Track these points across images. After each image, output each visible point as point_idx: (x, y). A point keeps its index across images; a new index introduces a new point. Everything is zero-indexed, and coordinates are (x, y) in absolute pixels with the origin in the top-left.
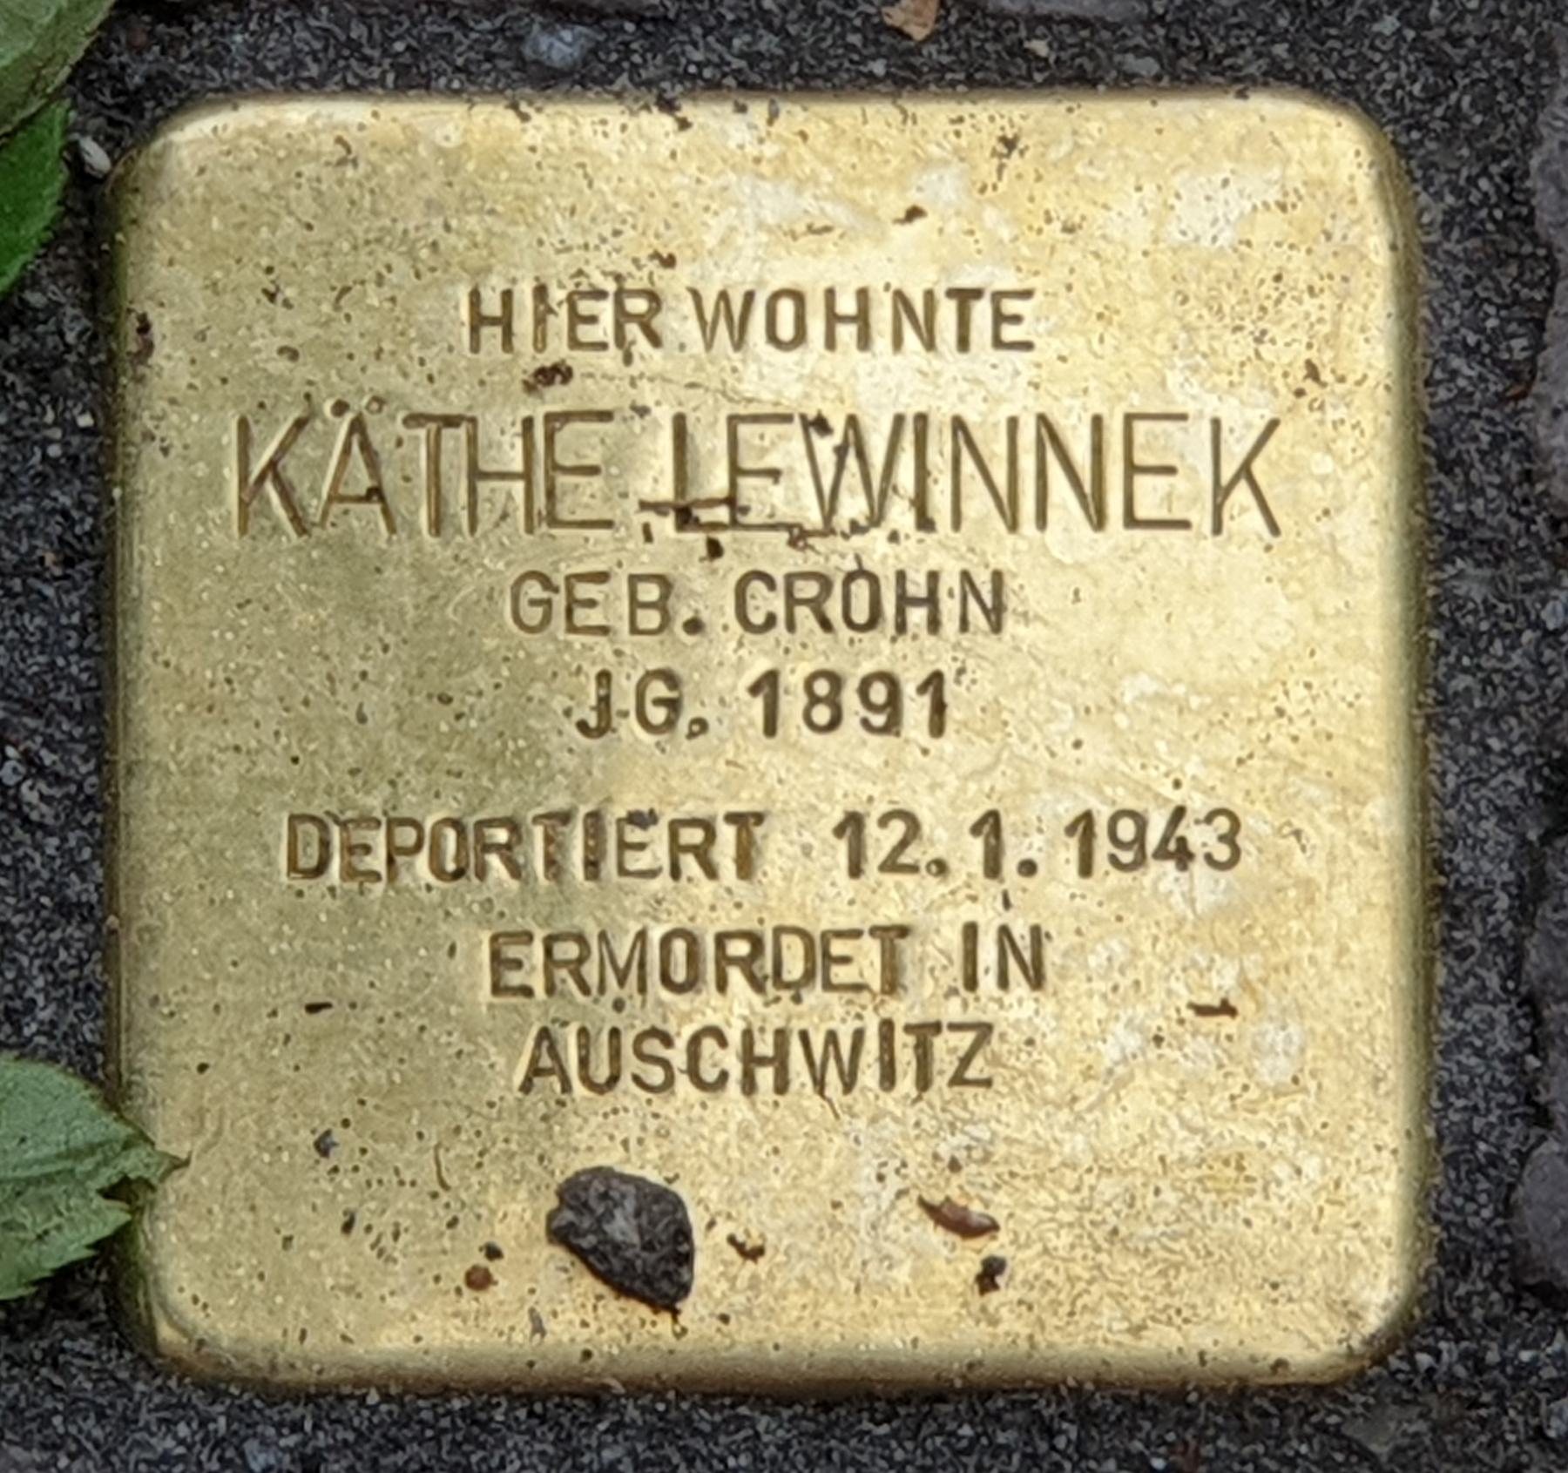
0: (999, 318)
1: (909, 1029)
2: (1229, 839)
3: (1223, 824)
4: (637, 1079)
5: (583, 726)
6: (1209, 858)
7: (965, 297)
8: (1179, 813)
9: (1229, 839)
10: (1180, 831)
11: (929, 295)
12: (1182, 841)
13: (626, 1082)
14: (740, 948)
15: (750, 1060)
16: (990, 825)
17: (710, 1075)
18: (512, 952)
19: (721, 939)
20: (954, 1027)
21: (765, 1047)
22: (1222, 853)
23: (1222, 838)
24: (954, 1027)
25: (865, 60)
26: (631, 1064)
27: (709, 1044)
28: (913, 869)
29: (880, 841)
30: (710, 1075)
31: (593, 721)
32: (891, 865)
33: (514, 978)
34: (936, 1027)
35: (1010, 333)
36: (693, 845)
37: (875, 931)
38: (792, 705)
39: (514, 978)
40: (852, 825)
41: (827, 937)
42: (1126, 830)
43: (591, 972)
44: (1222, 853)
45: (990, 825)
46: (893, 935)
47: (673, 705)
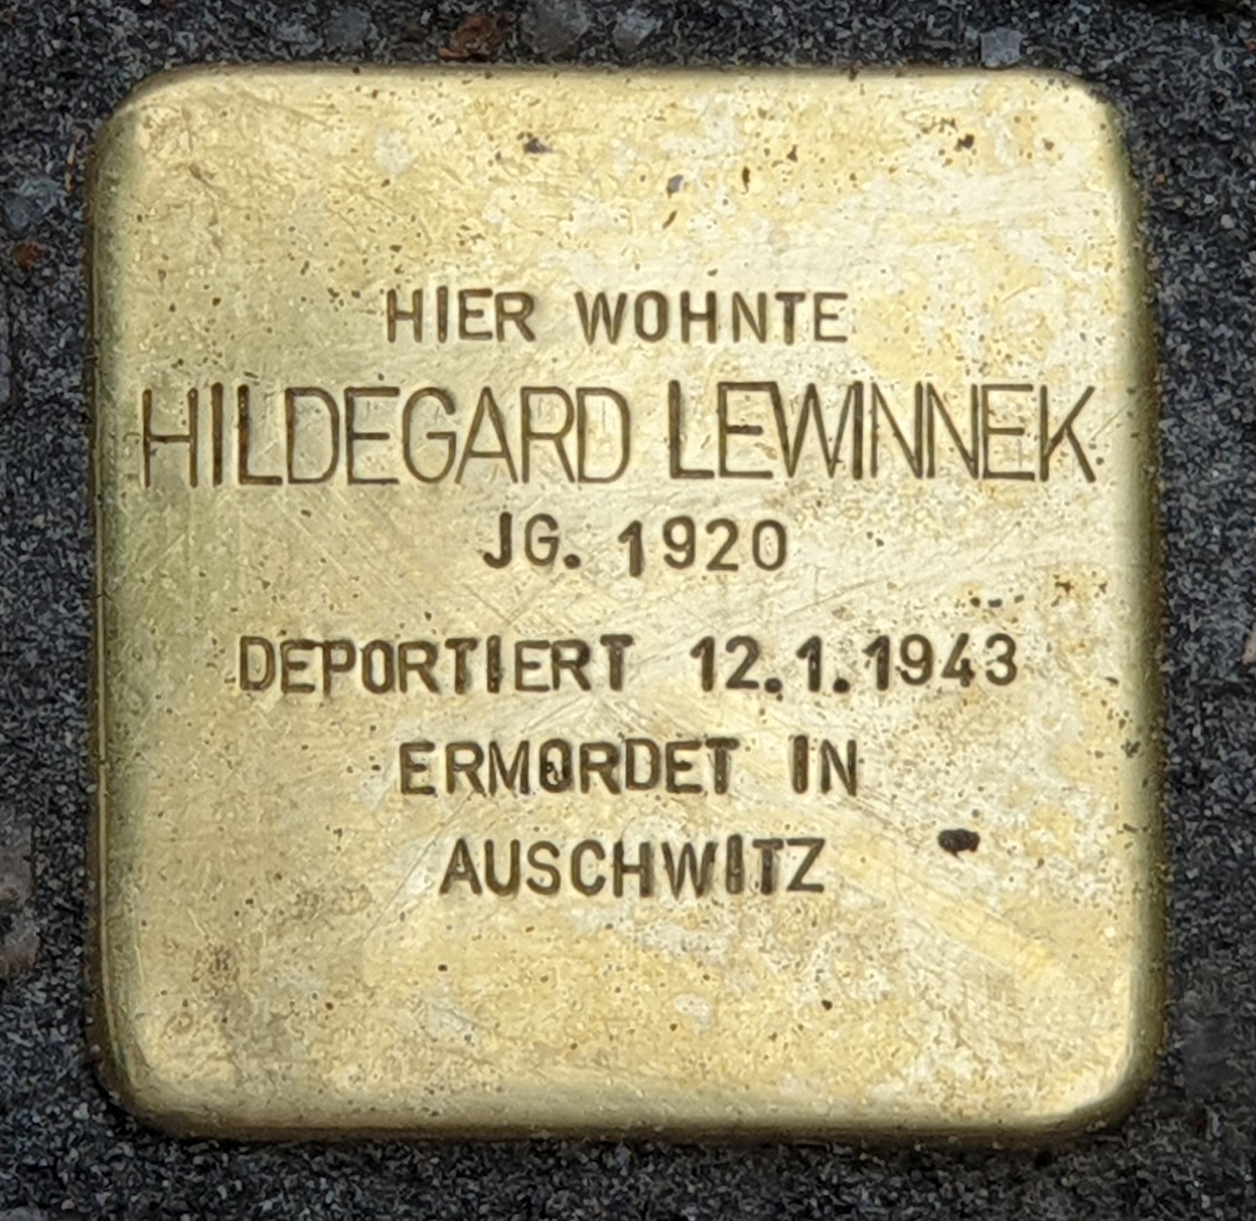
0: (819, 316)
1: (757, 843)
2: (1007, 659)
3: (1001, 648)
4: (531, 883)
5: (488, 558)
6: (991, 675)
7: (790, 299)
8: (963, 640)
9: (1007, 659)
10: (965, 654)
11: (762, 298)
12: (966, 663)
13: (524, 888)
14: (599, 757)
15: (621, 868)
16: (812, 650)
17: (588, 879)
18: (418, 757)
19: (585, 749)
20: (794, 842)
21: (632, 858)
22: (1001, 670)
23: (1001, 659)
24: (794, 842)
25: (1206, 699)
26: (527, 870)
27: (588, 855)
28: (753, 685)
29: (726, 666)
30: (588, 879)
31: (497, 553)
32: (736, 682)
33: (418, 779)
34: (778, 844)
35: (828, 328)
36: (573, 659)
37: (712, 742)
38: (654, 549)
39: (418, 779)
40: (705, 649)
41: (672, 747)
42: (916, 650)
43: (484, 773)
44: (1001, 670)
45: (812, 650)
46: (723, 746)
47: (554, 542)
